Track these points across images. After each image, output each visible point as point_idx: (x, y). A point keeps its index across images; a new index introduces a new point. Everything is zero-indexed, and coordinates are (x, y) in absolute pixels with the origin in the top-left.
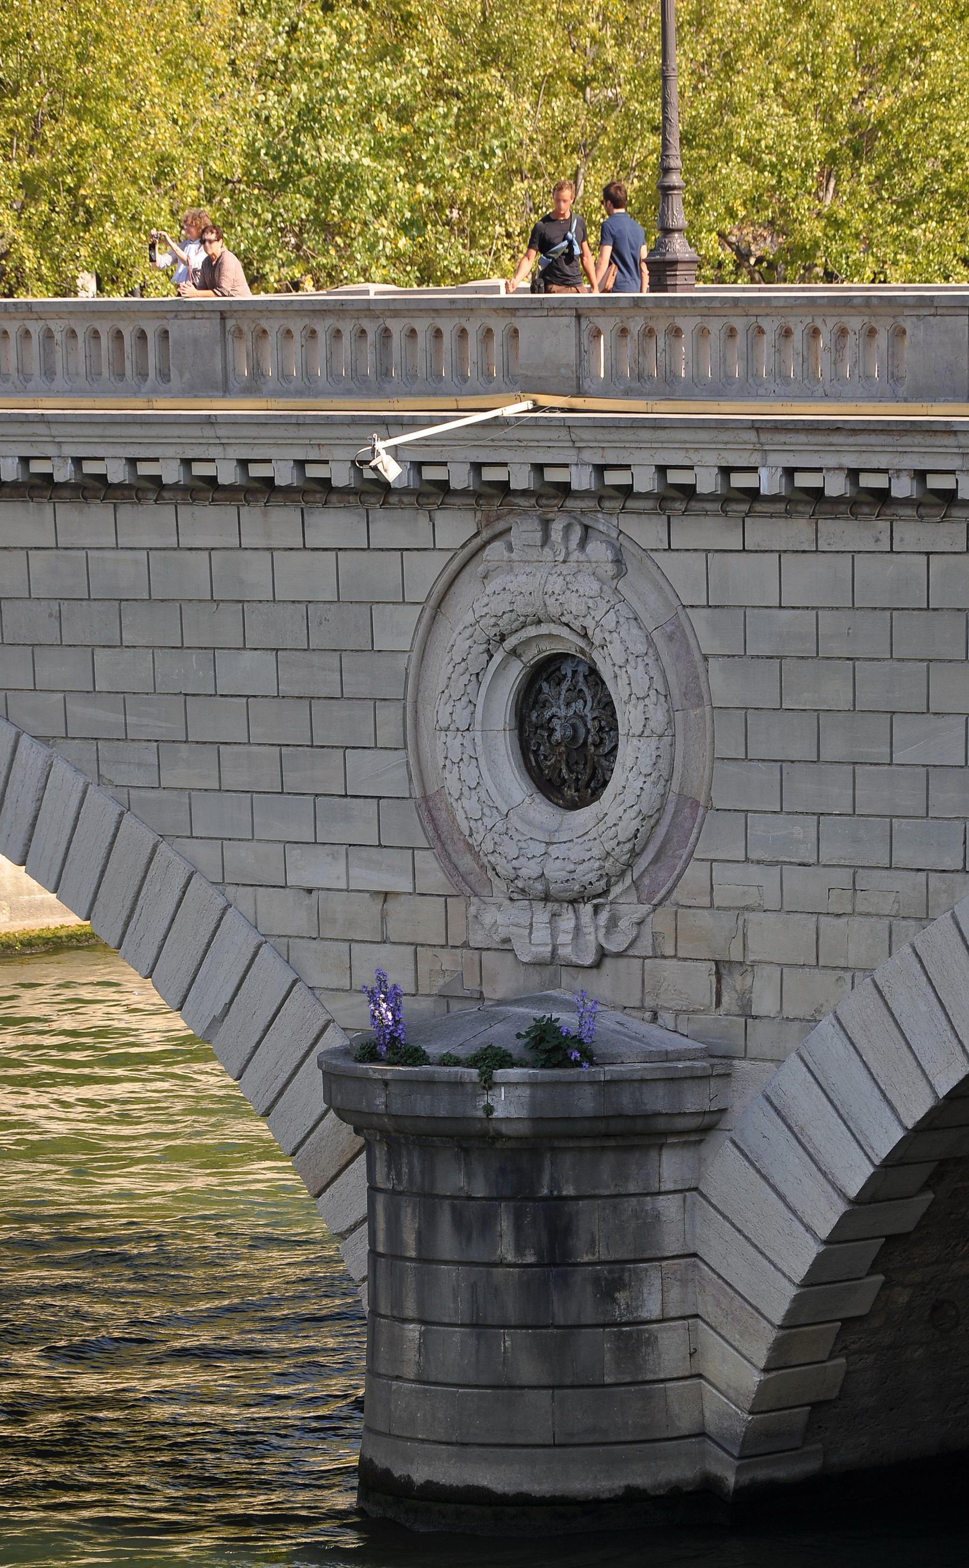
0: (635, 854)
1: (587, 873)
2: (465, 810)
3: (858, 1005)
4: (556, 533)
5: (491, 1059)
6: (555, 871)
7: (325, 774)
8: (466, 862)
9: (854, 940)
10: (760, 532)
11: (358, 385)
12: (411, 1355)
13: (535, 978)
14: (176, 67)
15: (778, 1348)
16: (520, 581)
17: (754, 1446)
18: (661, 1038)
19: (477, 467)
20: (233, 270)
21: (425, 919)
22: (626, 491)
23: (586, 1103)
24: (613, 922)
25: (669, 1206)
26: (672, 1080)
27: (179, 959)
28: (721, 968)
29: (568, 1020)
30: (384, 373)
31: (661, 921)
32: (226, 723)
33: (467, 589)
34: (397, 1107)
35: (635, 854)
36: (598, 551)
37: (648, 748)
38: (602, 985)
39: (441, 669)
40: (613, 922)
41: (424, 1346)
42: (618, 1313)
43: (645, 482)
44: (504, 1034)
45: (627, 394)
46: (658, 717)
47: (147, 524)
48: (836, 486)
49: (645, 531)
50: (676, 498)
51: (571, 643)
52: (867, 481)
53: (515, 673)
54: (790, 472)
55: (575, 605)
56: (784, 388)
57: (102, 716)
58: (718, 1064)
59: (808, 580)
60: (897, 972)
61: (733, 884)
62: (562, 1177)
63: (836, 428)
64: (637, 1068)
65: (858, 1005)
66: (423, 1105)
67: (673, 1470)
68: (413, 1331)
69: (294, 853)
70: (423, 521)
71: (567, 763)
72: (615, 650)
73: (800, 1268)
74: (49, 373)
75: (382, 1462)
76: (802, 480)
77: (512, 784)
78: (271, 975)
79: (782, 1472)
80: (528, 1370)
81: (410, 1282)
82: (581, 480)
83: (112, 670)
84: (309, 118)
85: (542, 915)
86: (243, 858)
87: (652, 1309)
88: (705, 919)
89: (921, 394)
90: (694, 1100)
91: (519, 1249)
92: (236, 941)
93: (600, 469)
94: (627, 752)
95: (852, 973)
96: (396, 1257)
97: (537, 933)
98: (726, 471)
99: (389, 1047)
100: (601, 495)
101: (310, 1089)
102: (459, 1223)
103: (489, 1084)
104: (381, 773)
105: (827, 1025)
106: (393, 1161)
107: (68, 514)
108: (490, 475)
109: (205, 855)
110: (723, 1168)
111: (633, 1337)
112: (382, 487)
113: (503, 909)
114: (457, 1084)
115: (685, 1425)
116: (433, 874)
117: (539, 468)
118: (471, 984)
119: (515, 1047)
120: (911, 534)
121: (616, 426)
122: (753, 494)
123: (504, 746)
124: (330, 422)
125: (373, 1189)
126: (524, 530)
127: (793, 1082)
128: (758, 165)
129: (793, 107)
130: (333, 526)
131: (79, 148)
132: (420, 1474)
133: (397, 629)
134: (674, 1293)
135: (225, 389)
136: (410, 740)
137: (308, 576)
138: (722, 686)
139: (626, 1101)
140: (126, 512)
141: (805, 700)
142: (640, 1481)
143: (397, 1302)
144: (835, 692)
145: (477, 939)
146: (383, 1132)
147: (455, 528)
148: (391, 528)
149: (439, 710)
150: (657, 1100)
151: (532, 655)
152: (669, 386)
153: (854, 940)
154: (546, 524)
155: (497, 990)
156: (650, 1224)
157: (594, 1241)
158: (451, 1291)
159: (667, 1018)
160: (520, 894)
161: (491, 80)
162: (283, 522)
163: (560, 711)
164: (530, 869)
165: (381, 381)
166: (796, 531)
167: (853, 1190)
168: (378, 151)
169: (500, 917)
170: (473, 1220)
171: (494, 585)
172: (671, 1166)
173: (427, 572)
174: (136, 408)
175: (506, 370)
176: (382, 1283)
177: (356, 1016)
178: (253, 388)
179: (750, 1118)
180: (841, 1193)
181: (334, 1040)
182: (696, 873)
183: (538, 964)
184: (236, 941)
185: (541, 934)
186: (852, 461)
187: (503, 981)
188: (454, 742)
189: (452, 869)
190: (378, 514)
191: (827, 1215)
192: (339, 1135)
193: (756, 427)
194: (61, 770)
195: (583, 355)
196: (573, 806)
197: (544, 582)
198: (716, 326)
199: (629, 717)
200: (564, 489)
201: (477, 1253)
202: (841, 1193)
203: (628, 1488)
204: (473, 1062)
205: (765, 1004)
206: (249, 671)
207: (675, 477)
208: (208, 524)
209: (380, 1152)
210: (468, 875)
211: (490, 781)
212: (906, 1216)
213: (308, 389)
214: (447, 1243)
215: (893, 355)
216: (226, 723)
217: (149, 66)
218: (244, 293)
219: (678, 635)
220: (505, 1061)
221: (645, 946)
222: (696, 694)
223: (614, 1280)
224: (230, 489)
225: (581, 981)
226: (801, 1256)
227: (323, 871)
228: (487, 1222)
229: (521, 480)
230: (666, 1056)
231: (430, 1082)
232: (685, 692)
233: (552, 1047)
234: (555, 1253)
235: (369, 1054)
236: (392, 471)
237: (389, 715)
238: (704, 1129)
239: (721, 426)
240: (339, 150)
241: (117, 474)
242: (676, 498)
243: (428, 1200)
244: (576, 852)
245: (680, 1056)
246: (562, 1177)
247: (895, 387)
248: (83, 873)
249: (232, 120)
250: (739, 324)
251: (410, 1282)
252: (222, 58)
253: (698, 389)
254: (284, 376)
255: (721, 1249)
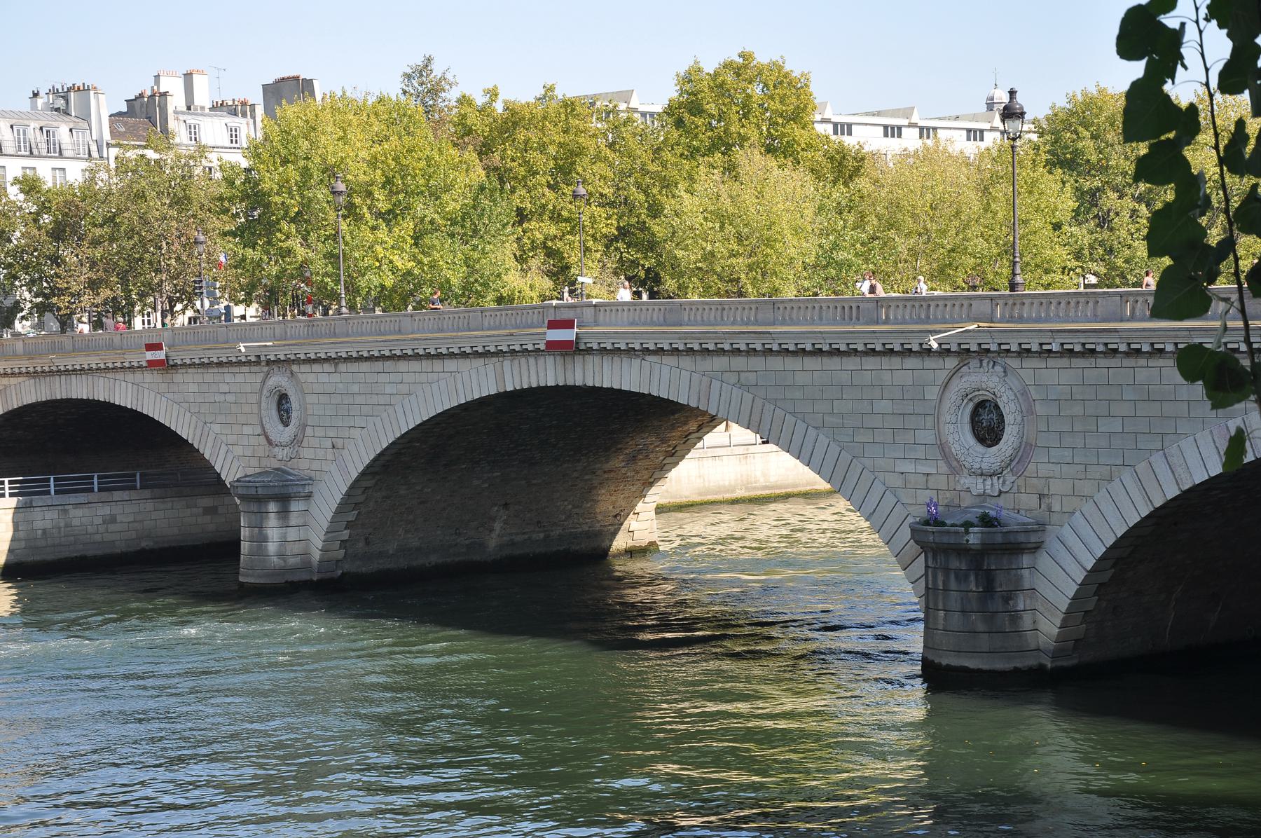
0: (1011, 461)
1: (996, 467)
2: (955, 448)
3: (1088, 508)
4: (985, 364)
5: (967, 525)
6: (985, 466)
8: (955, 464)
9: (1087, 488)
10: (1051, 362)
11: (920, 321)
12: (941, 621)
13: (978, 500)
14: (797, 231)
15: (1064, 621)
16: (973, 378)
17: (1057, 654)
18: (1022, 518)
19: (959, 344)
20: (879, 287)
21: (942, 482)
22: (1008, 351)
23: (999, 539)
24: (1004, 482)
25: (1026, 573)
26: (1026, 532)
27: (858, 496)
28: (1041, 496)
29: (992, 513)
30: (928, 317)
31: (1020, 481)
33: (955, 381)
34: (937, 540)
35: (1011, 461)
36: (998, 369)
37: (1016, 428)
39: (947, 405)
40: (1004, 482)
41: (945, 619)
42: (1010, 608)
43: (1014, 348)
44: (971, 517)
45: (1008, 322)
46: (1019, 419)
47: (851, 363)
48: (1078, 348)
49: (1014, 363)
50: (1024, 353)
51: (989, 396)
52: (1088, 346)
53: (971, 405)
54: (1062, 344)
55: (991, 385)
56: (1058, 319)
58: (1041, 527)
59: (1066, 376)
60: (1101, 497)
61: (1044, 470)
62: (991, 563)
63: (1078, 331)
64: (1016, 528)
66: (945, 539)
67: (1031, 662)
68: (941, 613)
69: (898, 462)
70: (941, 361)
72: (1005, 398)
73: (1071, 594)
74: (821, 318)
75: (930, 657)
76: (1066, 347)
78: (890, 500)
79: (1065, 663)
80: (981, 627)
81: (940, 597)
82: (994, 348)
84: (835, 247)
85: (980, 480)
86: (880, 463)
87: (1021, 607)
88: (1035, 481)
89: (1104, 320)
90: (1034, 538)
91: (977, 586)
92: (878, 489)
93: (1000, 344)
94: (1008, 430)
95: (1086, 498)
96: (935, 589)
97: (978, 486)
98: (1041, 344)
99: (933, 521)
100: (999, 352)
101: (906, 533)
102: (957, 577)
103: (967, 532)
104: (927, 437)
105: (1078, 514)
106: (934, 558)
107: (826, 360)
108: (963, 347)
109: (868, 462)
110: (1043, 561)
111: (1015, 616)
112: (929, 351)
113: (971, 478)
114: (957, 533)
115: (1033, 646)
116: (944, 468)
117: (980, 344)
118: (956, 502)
119: (975, 521)
120: (1102, 362)
121: (1005, 331)
122: (1050, 351)
123: (967, 428)
124: (913, 332)
125: (927, 567)
126: (974, 363)
127: (1067, 532)
128: (975, 257)
129: (987, 240)
130: (911, 363)
131: (767, 255)
132: (944, 662)
133: (932, 393)
134: (1028, 602)
135: (877, 323)
136: (936, 426)
138: (1040, 409)
139: (1012, 538)
140: (845, 359)
141: (1068, 413)
142: (1018, 665)
143: (936, 604)
144: (1078, 410)
145: (959, 488)
146: (932, 549)
147: (951, 363)
148: (930, 363)
149: (946, 417)
150: (1022, 538)
151: (976, 400)
152: (1021, 320)
153: (1087, 488)
154: (981, 361)
155: (964, 504)
156: (1019, 579)
157: (1002, 585)
158: (954, 600)
159: (1022, 512)
160: (973, 473)
161: (891, 233)
162: (896, 362)
163: (985, 417)
164: (977, 466)
165: (927, 320)
166: (1064, 362)
167: (1089, 568)
168: (856, 255)
169: (966, 481)
170: (961, 577)
171: (964, 379)
172: (1026, 560)
173: (942, 376)
174: (850, 328)
175: (968, 316)
176: (931, 597)
177: (921, 512)
178: (886, 322)
181: (910, 520)
182: (1031, 467)
183: (979, 495)
184: (878, 489)
185: (980, 486)
186: (1083, 341)
187: (967, 501)
188: (951, 427)
189: (950, 466)
190: (926, 359)
191: (1080, 577)
192: (913, 548)
193: (1051, 331)
194: (821, 436)
195: (993, 311)
196: (990, 446)
198: (1036, 301)
199: (1008, 419)
200: (988, 351)
201: (963, 587)
203: (1016, 668)
204: (962, 526)
205: (1056, 507)
206: (884, 406)
207: (1024, 346)
208: (871, 363)
209: (930, 555)
210: (955, 468)
211: (962, 440)
212: (1106, 577)
213: (904, 322)
214: (953, 585)
215: (1095, 308)
217: (787, 232)
218: (883, 295)
219: (1025, 393)
220: (973, 525)
221: (1015, 489)
222: (1031, 411)
223: (1008, 597)
224: (880, 352)
225: (994, 501)
226: (1071, 590)
227: (908, 467)
228: (966, 577)
229: (974, 348)
230: (1024, 524)
231: (948, 532)
232: (1028, 411)
233: (987, 521)
234: (989, 588)
235: (927, 523)
236: (935, 346)
237: (929, 420)
238: (1037, 547)
239: (1040, 331)
240: (841, 255)
241: (843, 348)
242: (1024, 353)
243: (947, 571)
244: (992, 460)
245: (1028, 524)
246: (991, 563)
247: (1095, 318)
248: (828, 468)
249: (811, 249)
250: (1044, 301)
251: (940, 597)
252: (809, 229)
253: (1030, 320)
254: (896, 318)
255: (1044, 588)
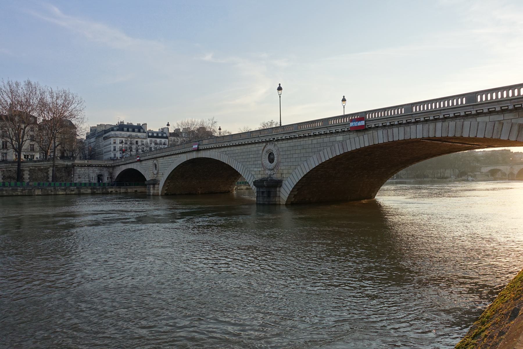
7: (256, 163)
9: (291, 171)
10: (284, 142)
21: (262, 172)
32: (250, 160)
38: (274, 176)
47: (246, 147)
49: (276, 143)
57: (242, 160)
59: (287, 145)
60: (302, 165)
61: (283, 168)
65: (291, 176)
71: (271, 160)
77: (268, 162)
83: (244, 157)
95: (290, 174)
97: (269, 172)
104: (260, 162)
126: (269, 144)
133: (261, 152)
136: (261, 160)
137: (255, 149)
138: (281, 153)
144: (289, 153)
147: (264, 144)
162: (254, 146)
166: (286, 142)
173: (263, 147)
179: (283, 184)
180: (280, 125)
197: (270, 147)
202: (280, 125)
206: (252, 156)
210: (265, 169)
216: (250, 160)
227: (256, 169)
232: (278, 155)
255: (281, 195)
